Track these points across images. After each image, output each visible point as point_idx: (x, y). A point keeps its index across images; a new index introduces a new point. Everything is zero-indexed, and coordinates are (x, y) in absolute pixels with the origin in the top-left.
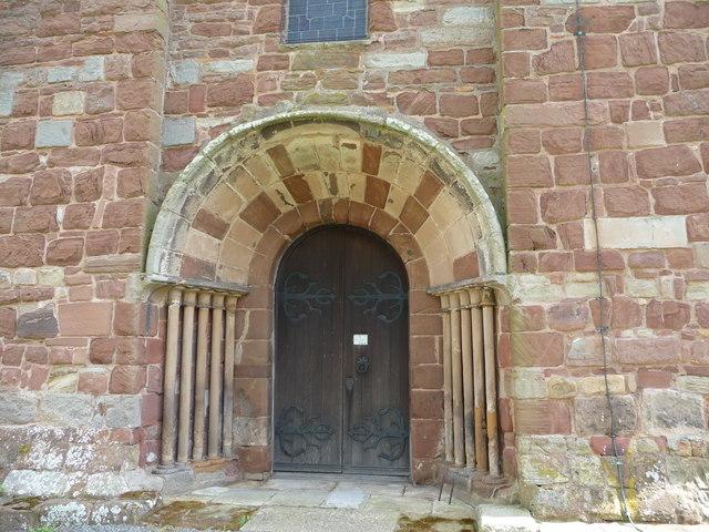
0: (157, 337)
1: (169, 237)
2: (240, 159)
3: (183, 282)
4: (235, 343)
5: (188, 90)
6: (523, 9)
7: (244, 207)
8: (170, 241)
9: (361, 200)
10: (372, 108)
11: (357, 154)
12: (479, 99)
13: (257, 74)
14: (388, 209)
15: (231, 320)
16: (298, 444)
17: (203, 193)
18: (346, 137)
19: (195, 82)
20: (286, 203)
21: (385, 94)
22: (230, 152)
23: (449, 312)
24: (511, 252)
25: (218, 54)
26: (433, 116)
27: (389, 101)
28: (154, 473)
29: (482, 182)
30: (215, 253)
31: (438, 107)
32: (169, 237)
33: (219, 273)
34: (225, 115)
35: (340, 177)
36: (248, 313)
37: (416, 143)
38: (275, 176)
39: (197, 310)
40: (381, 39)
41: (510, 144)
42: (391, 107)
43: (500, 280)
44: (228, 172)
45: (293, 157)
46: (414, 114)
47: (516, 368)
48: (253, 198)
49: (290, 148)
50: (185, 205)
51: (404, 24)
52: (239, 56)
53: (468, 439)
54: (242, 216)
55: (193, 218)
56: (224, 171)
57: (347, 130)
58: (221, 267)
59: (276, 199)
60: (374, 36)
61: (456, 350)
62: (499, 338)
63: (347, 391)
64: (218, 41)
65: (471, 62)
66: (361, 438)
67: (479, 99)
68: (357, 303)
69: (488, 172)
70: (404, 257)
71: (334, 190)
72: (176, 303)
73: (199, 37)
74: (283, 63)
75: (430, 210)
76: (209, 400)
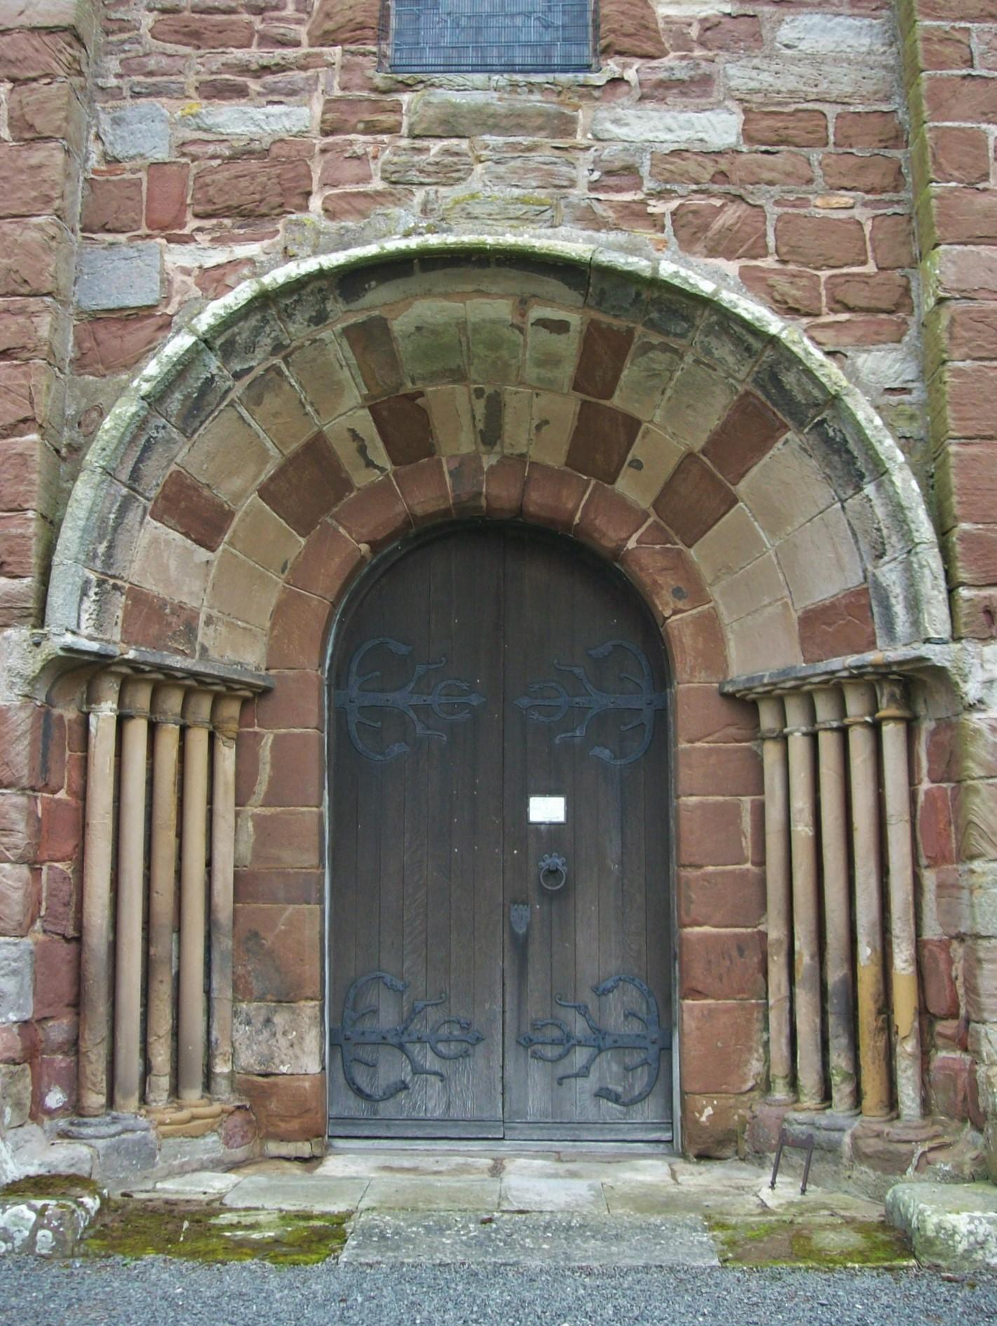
0: (62, 795)
1: (100, 539)
2: (278, 348)
3: (131, 654)
4: (237, 815)
5: (143, 175)
6: (967, 30)
7: (270, 469)
8: (102, 549)
9: (555, 458)
10: (613, 236)
11: (568, 346)
12: (867, 229)
13: (320, 142)
14: (624, 485)
15: (227, 757)
16: (392, 1069)
17: (183, 431)
18: (549, 301)
19: (161, 155)
20: (370, 464)
21: (643, 203)
22: (257, 331)
23: (784, 739)
24: (964, 592)
25: (217, 91)
26: (759, 263)
27: (655, 222)
28: (64, 1135)
29: (889, 425)
30: (196, 586)
31: (771, 241)
32: (100, 539)
33: (205, 635)
34: (238, 240)
35: (515, 398)
36: (268, 740)
37: (727, 321)
38: (354, 395)
39: (153, 728)
40: (630, 75)
41: (952, 338)
42: (659, 236)
43: (938, 655)
44: (247, 380)
45: (404, 348)
46: (712, 252)
47: (977, 865)
48: (294, 446)
49: (400, 325)
50: (140, 460)
51: (683, 43)
52: (276, 95)
53: (838, 1044)
54: (264, 493)
55: (153, 494)
56: (237, 376)
57: (553, 286)
58: (209, 621)
59: (345, 452)
60: (612, 66)
61: (802, 830)
62: (921, 798)
63: (514, 935)
64: (223, 59)
65: (844, 140)
66: (550, 1051)
67: (867, 229)
68: (536, 716)
69: (894, 399)
70: (665, 604)
71: (491, 434)
72: (106, 711)
73: (171, 48)
74: (387, 119)
75: (742, 488)
76: (179, 958)
